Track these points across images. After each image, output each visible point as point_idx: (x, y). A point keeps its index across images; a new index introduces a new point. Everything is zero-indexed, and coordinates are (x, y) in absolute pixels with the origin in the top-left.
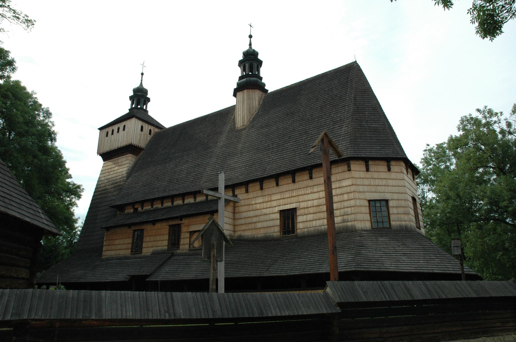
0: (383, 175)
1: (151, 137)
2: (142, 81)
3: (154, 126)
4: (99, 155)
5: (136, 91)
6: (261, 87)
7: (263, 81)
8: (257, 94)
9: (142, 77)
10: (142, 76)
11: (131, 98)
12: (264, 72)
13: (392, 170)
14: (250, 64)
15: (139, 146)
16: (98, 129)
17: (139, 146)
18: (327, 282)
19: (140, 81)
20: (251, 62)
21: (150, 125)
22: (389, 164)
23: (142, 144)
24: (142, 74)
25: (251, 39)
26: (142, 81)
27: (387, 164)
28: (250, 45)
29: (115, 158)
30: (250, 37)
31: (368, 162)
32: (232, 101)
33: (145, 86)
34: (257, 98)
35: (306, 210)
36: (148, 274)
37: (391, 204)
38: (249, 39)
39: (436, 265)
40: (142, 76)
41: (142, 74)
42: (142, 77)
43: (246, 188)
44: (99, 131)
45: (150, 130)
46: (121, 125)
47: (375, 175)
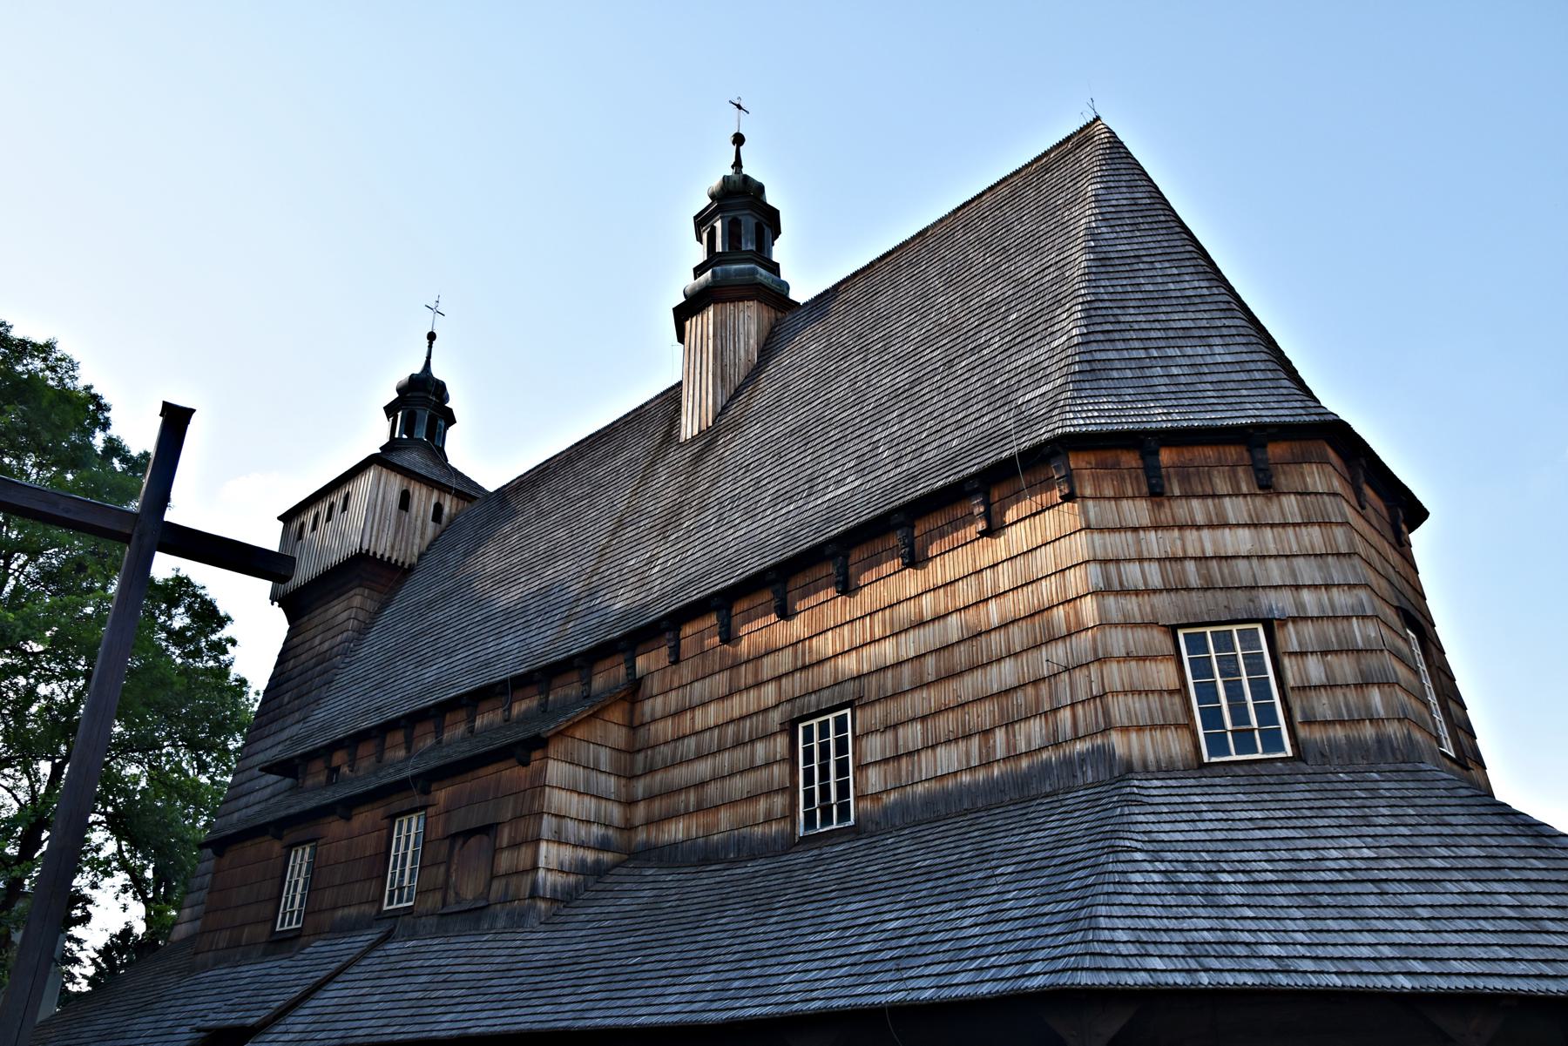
0: (1234, 509)
1: (438, 531)
2: (429, 358)
3: (450, 493)
4: (276, 604)
6: (775, 297)
7: (785, 275)
8: (749, 319)
9: (430, 347)
11: (390, 410)
12: (780, 251)
13: (1282, 482)
14: (730, 222)
15: (389, 558)
16: (280, 518)
17: (389, 558)
18: (90, 988)
21: (439, 490)
22: (1259, 456)
23: (407, 553)
24: (432, 337)
26: (429, 358)
27: (1252, 456)
28: (738, 164)
29: (317, 609)
31: (1156, 453)
33: (437, 372)
34: (753, 329)
35: (892, 705)
36: (251, 1021)
37: (1290, 637)
39: (1113, 206)
41: (432, 337)
42: (430, 347)
43: (672, 644)
44: (281, 524)
45: (438, 508)
46: (338, 498)
47: (1198, 510)
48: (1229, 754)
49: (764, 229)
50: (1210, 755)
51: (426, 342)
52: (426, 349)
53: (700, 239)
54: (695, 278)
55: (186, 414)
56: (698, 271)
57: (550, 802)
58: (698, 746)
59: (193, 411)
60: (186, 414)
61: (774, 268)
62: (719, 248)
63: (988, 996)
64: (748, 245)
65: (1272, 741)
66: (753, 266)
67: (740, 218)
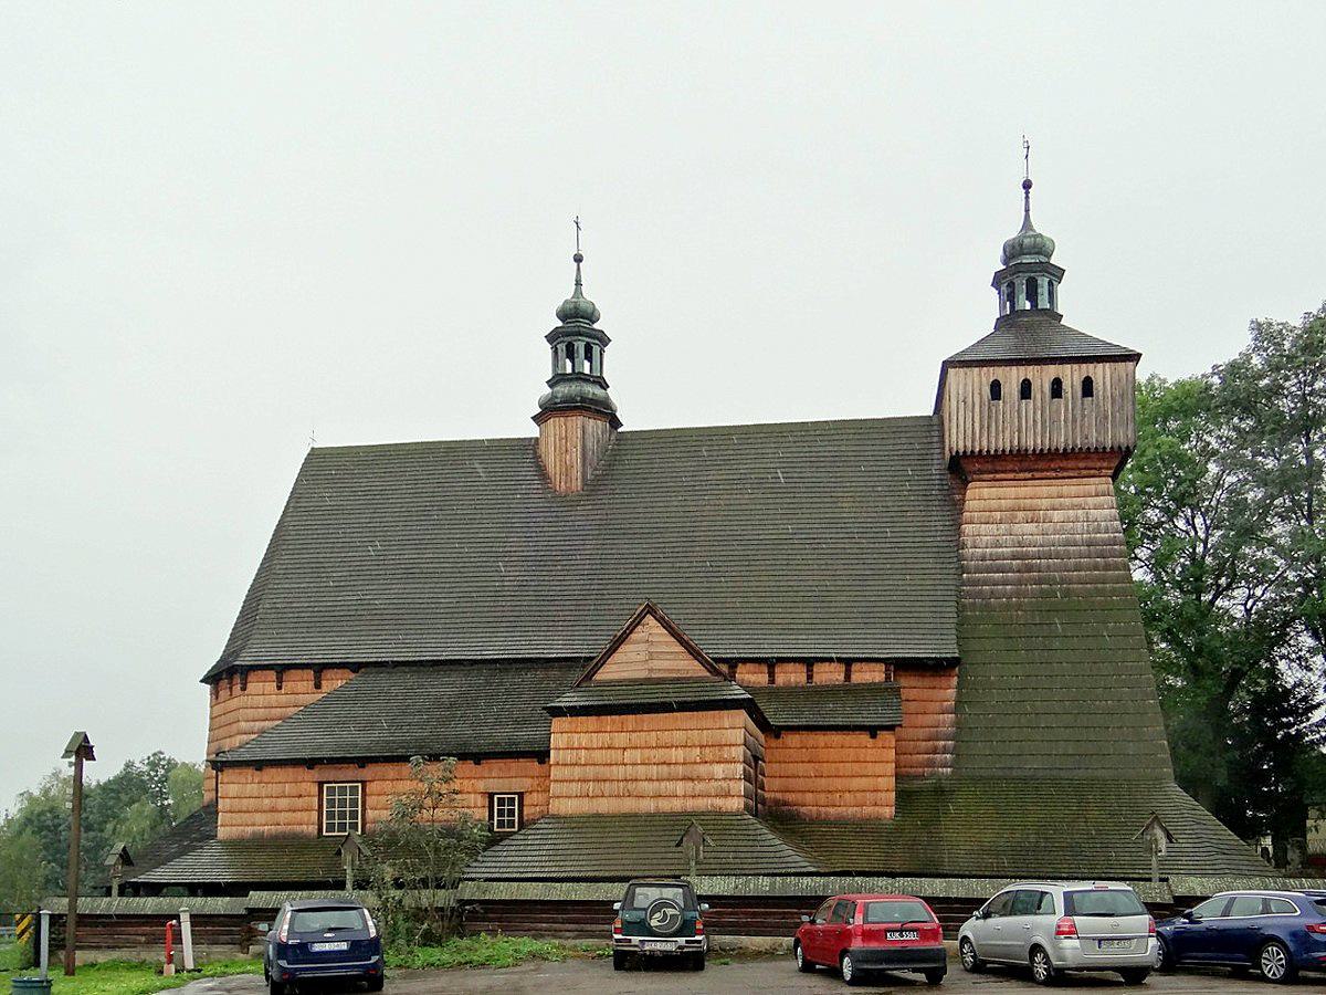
2: (1027, 211)
5: (1013, 251)
9: (1027, 197)
10: (1027, 193)
19: (1023, 213)
20: (569, 339)
24: (1027, 185)
26: (1027, 211)
28: (578, 283)
30: (578, 259)
32: (533, 431)
37: (527, 801)
38: (576, 264)
40: (1027, 193)
41: (1027, 185)
42: (1027, 197)
58: (292, 688)
60: (1053, 397)
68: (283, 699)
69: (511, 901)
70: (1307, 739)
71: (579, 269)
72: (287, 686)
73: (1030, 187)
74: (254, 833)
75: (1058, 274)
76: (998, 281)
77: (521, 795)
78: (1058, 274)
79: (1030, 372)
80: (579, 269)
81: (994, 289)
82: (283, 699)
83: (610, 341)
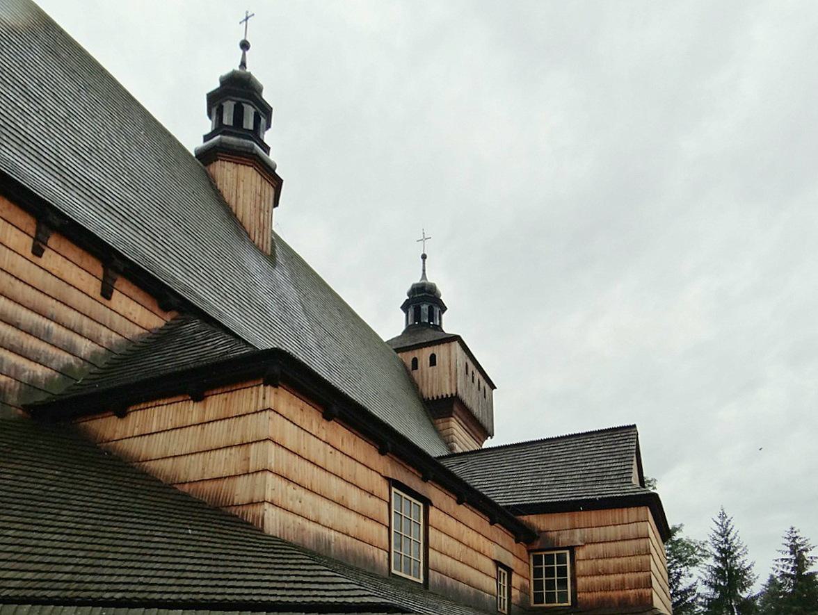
2: (424, 270)
9: (424, 263)
10: (424, 261)
19: (421, 272)
20: (239, 99)
24: (424, 257)
25: (247, 53)
26: (424, 270)
28: (243, 64)
38: (241, 52)
40: (424, 261)
41: (424, 257)
42: (424, 263)
48: (543, 603)
49: (260, 119)
50: (566, 554)
51: (421, 260)
52: (422, 265)
53: (210, 115)
54: (205, 141)
55: (431, 365)
56: (207, 138)
57: (269, 525)
59: (496, 388)
60: (431, 365)
61: (266, 149)
62: (225, 122)
63: (353, 604)
64: (249, 124)
65: (563, 597)
66: (252, 142)
67: (244, 105)
68: (38, 276)
69: (461, 480)
70: (696, 610)
71: (244, 55)
72: (50, 259)
73: (426, 258)
74: (318, 539)
75: (443, 309)
76: (405, 307)
77: (572, 549)
78: (443, 309)
79: (416, 354)
80: (244, 55)
81: (402, 312)
82: (38, 276)
83: (401, 308)
